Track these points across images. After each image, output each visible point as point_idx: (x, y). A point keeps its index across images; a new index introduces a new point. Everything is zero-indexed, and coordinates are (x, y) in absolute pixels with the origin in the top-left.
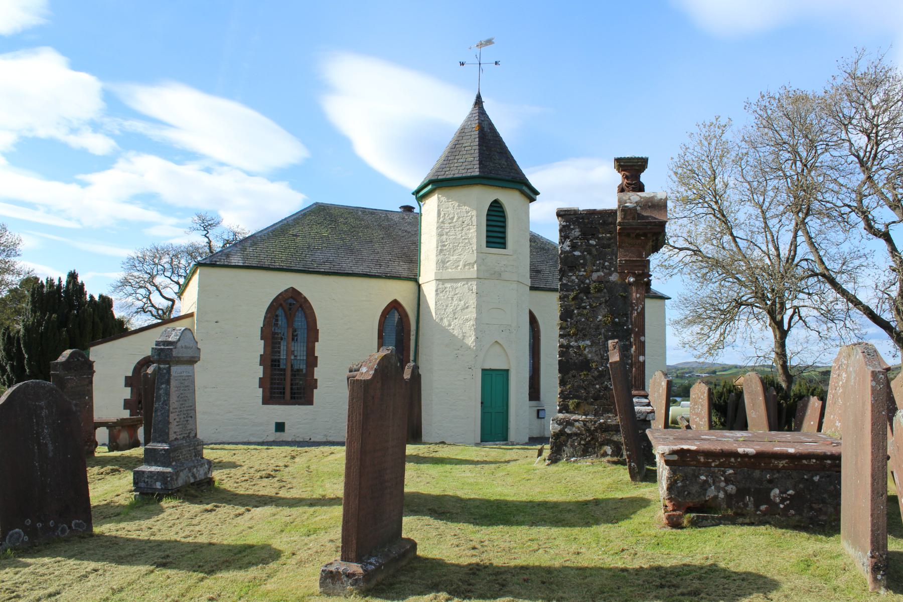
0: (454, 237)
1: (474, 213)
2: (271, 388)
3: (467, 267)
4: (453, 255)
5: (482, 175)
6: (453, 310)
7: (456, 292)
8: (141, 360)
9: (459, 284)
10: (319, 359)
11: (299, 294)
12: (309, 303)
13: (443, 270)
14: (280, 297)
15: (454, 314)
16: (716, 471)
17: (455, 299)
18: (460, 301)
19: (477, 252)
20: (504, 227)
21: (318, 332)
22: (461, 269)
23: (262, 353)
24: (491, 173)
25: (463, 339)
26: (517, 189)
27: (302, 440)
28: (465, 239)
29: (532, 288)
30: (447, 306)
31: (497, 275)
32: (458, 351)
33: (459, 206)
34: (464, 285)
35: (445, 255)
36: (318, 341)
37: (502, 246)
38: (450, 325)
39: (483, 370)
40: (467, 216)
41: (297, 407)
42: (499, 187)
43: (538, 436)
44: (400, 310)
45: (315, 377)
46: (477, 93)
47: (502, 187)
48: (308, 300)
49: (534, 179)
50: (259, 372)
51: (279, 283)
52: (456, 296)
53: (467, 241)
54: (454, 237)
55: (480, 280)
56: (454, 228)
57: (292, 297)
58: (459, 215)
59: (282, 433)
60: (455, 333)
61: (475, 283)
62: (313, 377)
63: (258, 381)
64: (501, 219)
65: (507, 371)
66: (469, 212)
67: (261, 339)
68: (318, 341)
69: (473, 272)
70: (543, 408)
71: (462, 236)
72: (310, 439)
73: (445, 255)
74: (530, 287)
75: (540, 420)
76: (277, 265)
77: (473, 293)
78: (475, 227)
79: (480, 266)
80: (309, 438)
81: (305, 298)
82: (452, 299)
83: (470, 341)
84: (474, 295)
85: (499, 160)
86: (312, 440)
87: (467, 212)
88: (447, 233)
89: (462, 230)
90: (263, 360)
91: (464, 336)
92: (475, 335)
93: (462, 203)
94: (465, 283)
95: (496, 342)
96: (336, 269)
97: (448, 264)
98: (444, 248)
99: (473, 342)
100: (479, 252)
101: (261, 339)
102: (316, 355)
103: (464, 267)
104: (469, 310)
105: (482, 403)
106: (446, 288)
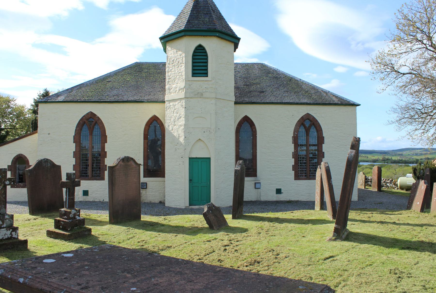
0: (174, 72)
1: (184, 55)
2: (86, 171)
3: (180, 91)
5: (187, 29)
6: (174, 120)
8: (16, 156)
9: (177, 103)
11: (95, 115)
13: (169, 94)
14: (84, 118)
15: (175, 122)
17: (175, 112)
18: (177, 113)
19: (185, 81)
20: (207, 62)
21: (107, 137)
22: (177, 92)
23: (75, 151)
24: (193, 27)
25: (179, 138)
26: (215, 36)
28: (179, 73)
29: (236, 103)
31: (200, 95)
32: (176, 146)
33: (177, 52)
34: (179, 103)
35: (170, 84)
36: (106, 142)
37: (206, 75)
38: (172, 130)
39: (190, 158)
40: (180, 58)
42: (201, 36)
44: (158, 121)
45: (105, 164)
47: (204, 36)
48: (100, 119)
49: (237, 30)
50: (292, 162)
53: (180, 74)
54: (174, 72)
56: (174, 67)
60: (175, 135)
61: (184, 101)
62: (104, 164)
64: (205, 57)
65: (209, 159)
66: (181, 55)
68: (106, 142)
69: (182, 95)
70: (259, 182)
71: (178, 71)
72: (104, 200)
73: (170, 84)
74: (235, 102)
75: (257, 190)
76: (87, 99)
77: (183, 108)
78: (184, 64)
80: (103, 199)
81: (98, 117)
82: (174, 113)
83: (182, 140)
84: (184, 109)
85: (204, 18)
87: (180, 55)
88: (171, 70)
91: (179, 136)
92: (184, 135)
94: (179, 101)
95: (200, 139)
96: (120, 99)
98: (170, 80)
100: (187, 80)
101: (74, 142)
103: (179, 91)
105: (190, 180)
106: (170, 106)
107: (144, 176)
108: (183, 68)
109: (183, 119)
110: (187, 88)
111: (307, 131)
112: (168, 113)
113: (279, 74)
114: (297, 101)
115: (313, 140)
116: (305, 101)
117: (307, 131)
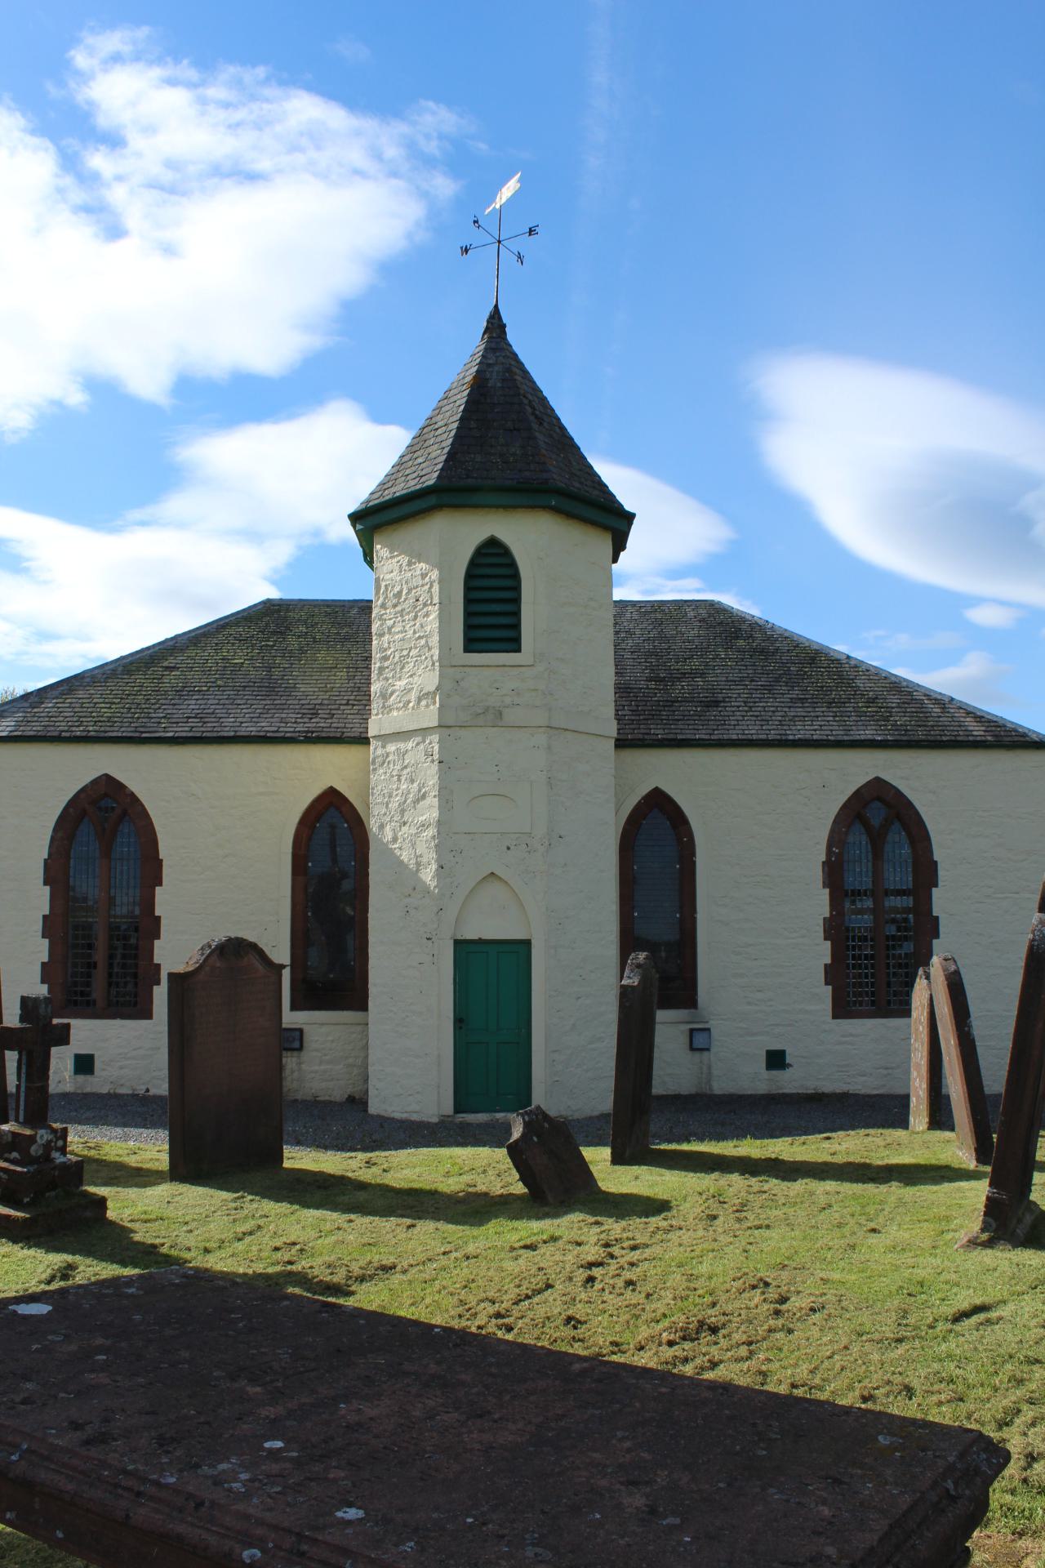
0: (401, 636)
1: (435, 575)
3: (424, 703)
4: (400, 679)
7: (405, 764)
9: (410, 744)
10: (163, 922)
12: (143, 806)
15: (403, 812)
16: (580, 1350)
19: (440, 666)
22: (413, 708)
25: (418, 870)
27: (130, 1092)
29: (621, 744)
30: (390, 797)
31: (493, 716)
33: (410, 564)
34: (418, 744)
36: (160, 884)
38: (395, 840)
40: (423, 586)
41: (118, 1022)
43: (693, 1091)
46: (491, 307)
51: (86, 764)
52: (405, 772)
53: (423, 642)
54: (401, 636)
55: (448, 731)
56: (402, 616)
57: (106, 795)
58: (410, 585)
59: (89, 1078)
63: (38, 969)
65: (527, 943)
67: (45, 883)
69: (430, 715)
70: (706, 1026)
71: (415, 632)
73: (387, 679)
74: (617, 740)
75: (697, 1054)
77: (433, 761)
78: (437, 607)
79: (449, 696)
80: (144, 1088)
83: (428, 875)
84: (435, 767)
86: (151, 1093)
87: (423, 576)
88: (390, 629)
89: (416, 617)
90: (50, 927)
91: (418, 864)
92: (437, 861)
93: (417, 556)
94: (419, 739)
95: (492, 873)
97: (392, 699)
99: (433, 877)
100: (445, 663)
101: (45, 883)
102: (157, 914)
104: (428, 801)
107: (295, 1007)
108: (432, 622)
109: (432, 801)
110: (450, 688)
111: (877, 841)
112: (379, 779)
113: (770, 639)
114: (838, 734)
115: (898, 876)
116: (868, 733)
117: (877, 841)
